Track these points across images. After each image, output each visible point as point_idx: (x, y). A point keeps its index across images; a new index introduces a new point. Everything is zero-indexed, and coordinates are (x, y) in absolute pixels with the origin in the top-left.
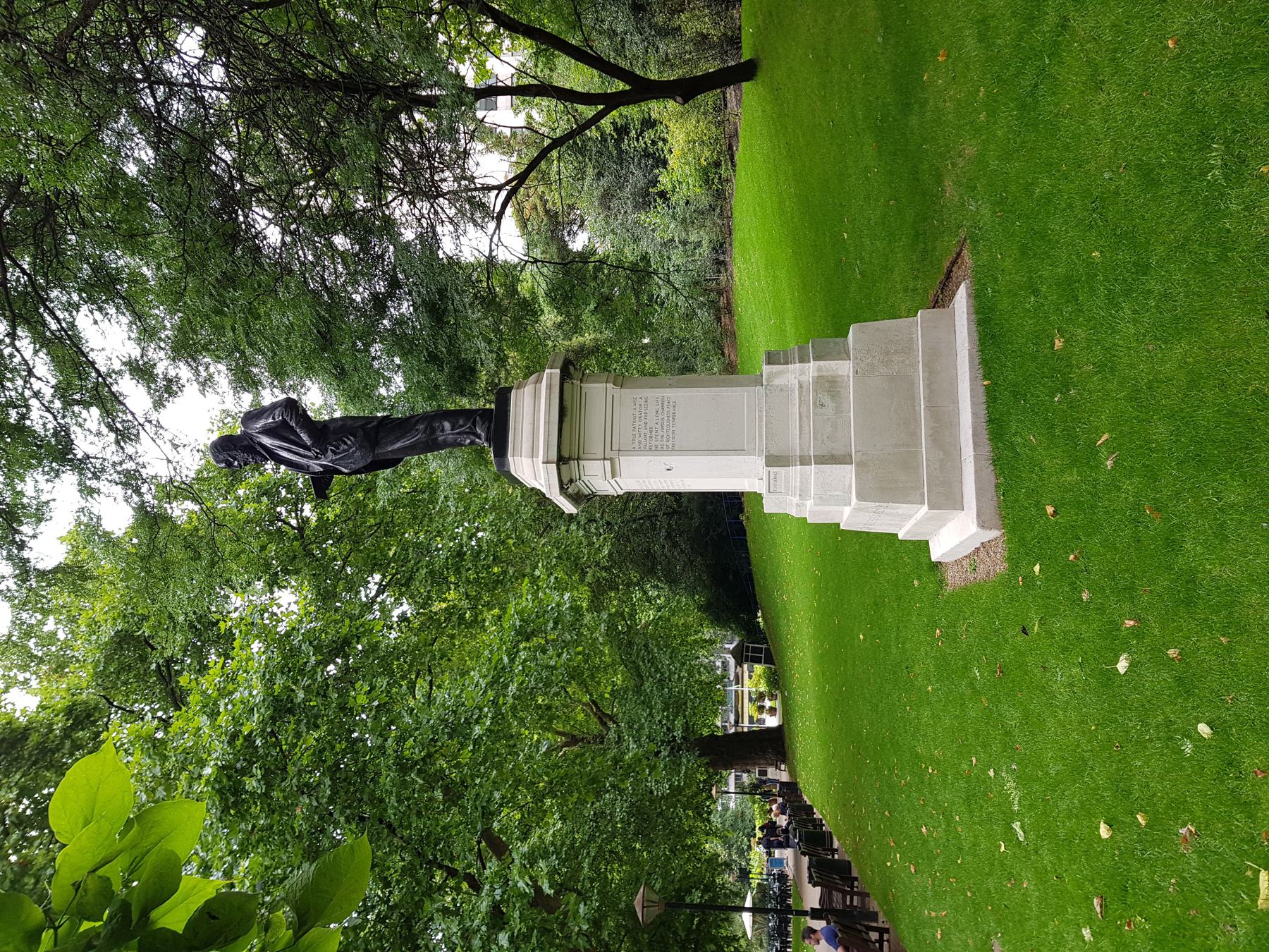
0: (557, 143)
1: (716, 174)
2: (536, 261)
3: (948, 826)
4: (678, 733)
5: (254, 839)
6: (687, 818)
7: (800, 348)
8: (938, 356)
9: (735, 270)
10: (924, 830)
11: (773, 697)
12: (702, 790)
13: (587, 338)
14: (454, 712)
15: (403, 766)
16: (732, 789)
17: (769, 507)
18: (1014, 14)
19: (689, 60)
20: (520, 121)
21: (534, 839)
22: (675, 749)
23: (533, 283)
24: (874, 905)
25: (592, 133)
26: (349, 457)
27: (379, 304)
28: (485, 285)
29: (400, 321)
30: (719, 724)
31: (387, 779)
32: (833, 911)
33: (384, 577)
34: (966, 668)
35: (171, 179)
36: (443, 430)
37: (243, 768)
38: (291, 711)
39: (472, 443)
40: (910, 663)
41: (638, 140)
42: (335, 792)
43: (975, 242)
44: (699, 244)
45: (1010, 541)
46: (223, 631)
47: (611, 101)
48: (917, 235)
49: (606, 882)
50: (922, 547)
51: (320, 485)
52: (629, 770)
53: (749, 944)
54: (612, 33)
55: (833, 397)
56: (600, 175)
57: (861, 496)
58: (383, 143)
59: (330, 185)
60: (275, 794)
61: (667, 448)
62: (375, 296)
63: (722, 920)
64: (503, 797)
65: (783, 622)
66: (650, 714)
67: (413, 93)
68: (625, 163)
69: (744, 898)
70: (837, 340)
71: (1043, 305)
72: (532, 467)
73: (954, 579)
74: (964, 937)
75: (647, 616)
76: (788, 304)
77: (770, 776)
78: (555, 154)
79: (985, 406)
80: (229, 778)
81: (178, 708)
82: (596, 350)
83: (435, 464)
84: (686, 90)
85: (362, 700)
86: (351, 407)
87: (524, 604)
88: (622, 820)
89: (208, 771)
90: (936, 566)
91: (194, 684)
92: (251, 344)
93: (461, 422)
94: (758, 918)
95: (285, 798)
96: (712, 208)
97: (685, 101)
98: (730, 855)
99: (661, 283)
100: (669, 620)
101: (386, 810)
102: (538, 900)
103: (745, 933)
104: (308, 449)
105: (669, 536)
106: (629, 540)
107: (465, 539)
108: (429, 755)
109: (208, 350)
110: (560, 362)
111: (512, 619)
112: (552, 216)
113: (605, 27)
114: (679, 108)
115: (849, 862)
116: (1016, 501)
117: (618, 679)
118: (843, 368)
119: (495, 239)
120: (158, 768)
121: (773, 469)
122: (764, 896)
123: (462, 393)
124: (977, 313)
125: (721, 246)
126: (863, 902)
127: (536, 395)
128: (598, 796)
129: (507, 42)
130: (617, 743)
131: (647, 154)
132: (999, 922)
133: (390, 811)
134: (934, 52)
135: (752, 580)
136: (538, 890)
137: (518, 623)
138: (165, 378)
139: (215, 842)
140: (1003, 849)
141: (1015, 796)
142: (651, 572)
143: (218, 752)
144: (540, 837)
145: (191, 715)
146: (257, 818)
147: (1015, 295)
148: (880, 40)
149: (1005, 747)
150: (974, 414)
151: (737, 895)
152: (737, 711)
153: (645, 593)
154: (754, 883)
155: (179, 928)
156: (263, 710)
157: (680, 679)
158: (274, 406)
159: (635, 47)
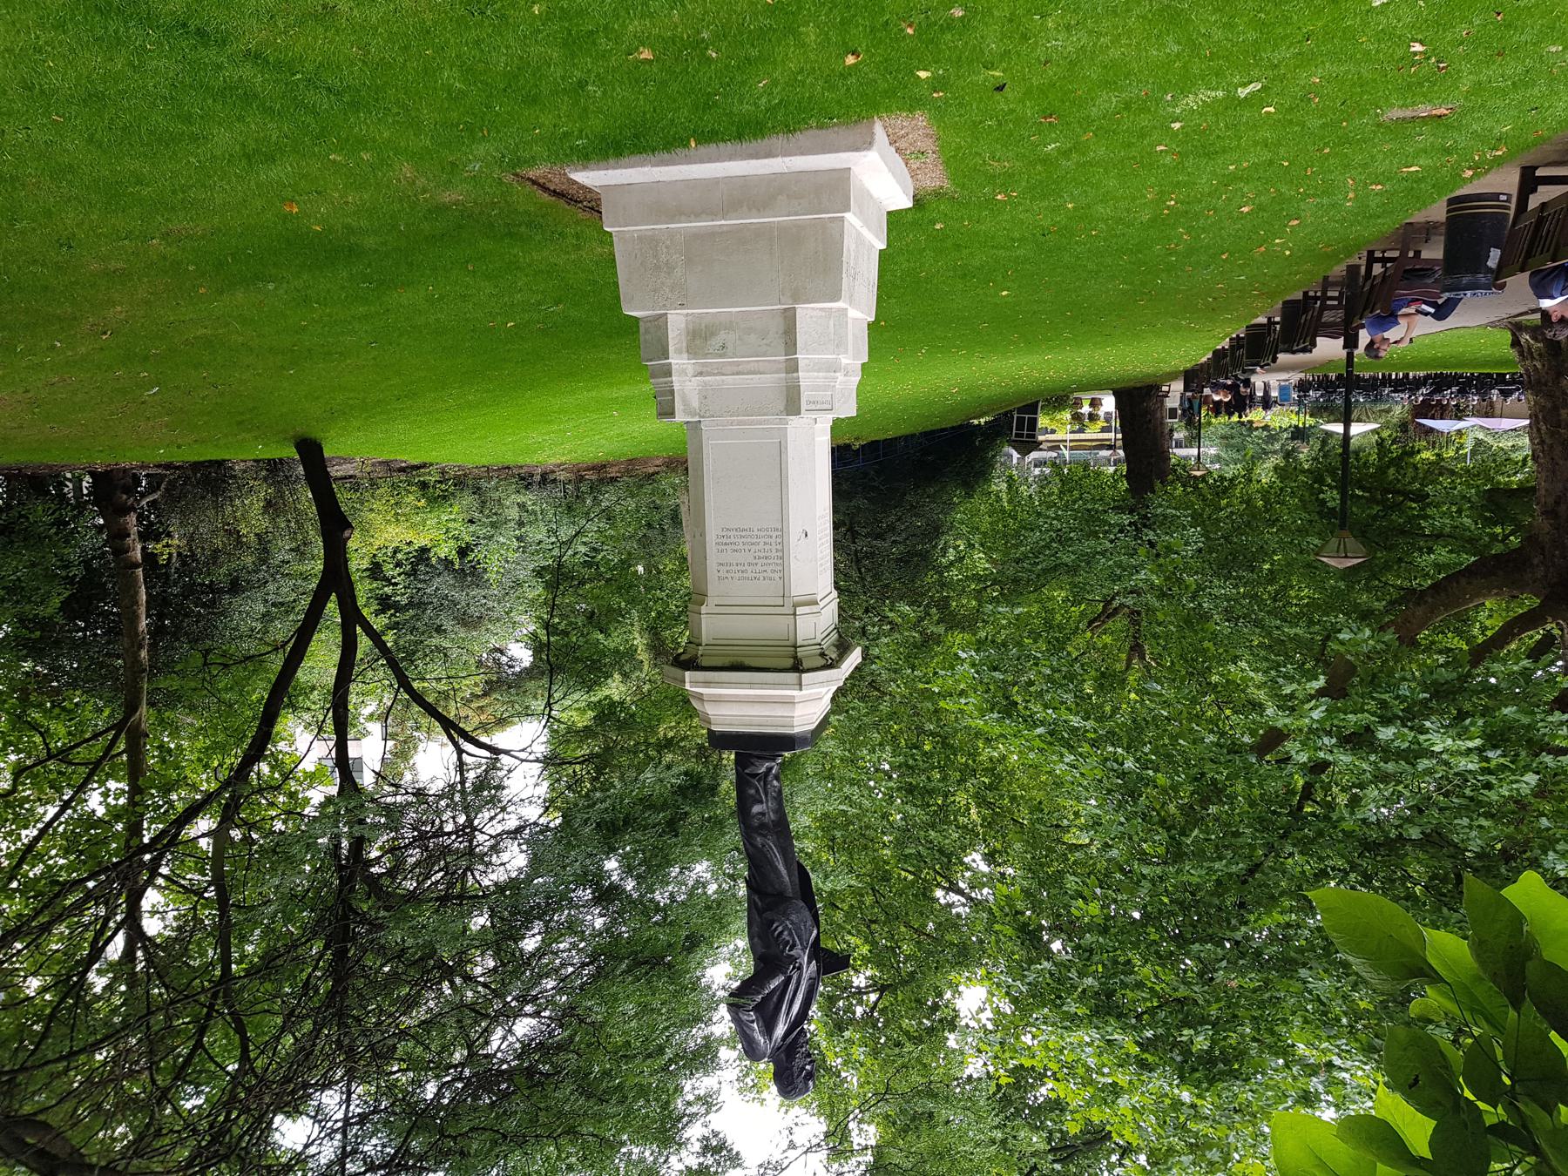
0: (404, 683)
1: (438, 487)
2: (549, 705)
3: (1241, 179)
4: (1126, 519)
5: (1269, 1040)
6: (1231, 506)
7: (653, 376)
8: (663, 204)
9: (553, 461)
10: (1245, 209)
11: (1078, 403)
12: (1196, 488)
13: (639, 641)
14: (1109, 792)
15: (1176, 854)
16: (1194, 451)
17: (849, 410)
18: (240, 119)
19: (297, 522)
20: (376, 728)
21: (1261, 695)
22: (1146, 522)
23: (575, 708)
24: (1339, 270)
25: (389, 638)
26: (798, 929)
27: (606, 895)
28: (578, 767)
29: (628, 870)
30: (1112, 469)
31: (1193, 873)
32: (1347, 321)
33: (938, 885)
34: (1046, 160)
35: (462, 1154)
36: (763, 814)
37: (1181, 1053)
38: (1110, 994)
39: (777, 777)
40: (1038, 232)
41: (396, 584)
42: (1210, 938)
43: (519, 162)
44: (522, 506)
45: (888, 109)
46: (1011, 1080)
47: (351, 617)
48: (510, 235)
49: (1313, 605)
50: (895, 220)
51: (833, 963)
52: (1173, 579)
53: (1386, 426)
54: (267, 618)
55: (713, 334)
56: (439, 630)
57: (836, 296)
58: (412, 897)
59: (463, 959)
60: (1214, 1011)
61: (778, 538)
62: (597, 901)
63: (1358, 460)
64: (1211, 731)
65: (985, 392)
66: (1103, 553)
67: (347, 858)
68: (425, 599)
69: (1329, 434)
70: (642, 330)
71: (598, 75)
72: (806, 704)
73: (935, 179)
74: (1381, 156)
75: (980, 562)
76: (594, 394)
77: (1176, 405)
78: (415, 685)
79: (722, 145)
80: (1194, 1070)
81: (1108, 1136)
82: (653, 631)
83: (800, 821)
84: (335, 526)
85: (1094, 908)
86: (733, 928)
87: (971, 707)
88: (1236, 586)
89: (1186, 1096)
90: (917, 201)
91: (1077, 1116)
92: (661, 1050)
93: (752, 792)
94: (1355, 415)
95: (1218, 1000)
96: (477, 490)
97: (349, 526)
98: (1275, 452)
99: (570, 552)
100: (984, 534)
101: (1230, 875)
102: (1335, 690)
103: (1374, 431)
104: (789, 979)
105: (880, 536)
106: (887, 586)
107: (891, 784)
108: (1162, 822)
109: (667, 1103)
110: (677, 672)
111: (989, 723)
112: (490, 687)
113: (259, 626)
114: (357, 533)
115: (1285, 303)
116: (839, 102)
117: (1060, 595)
118: (677, 322)
119: (523, 755)
120: (1183, 1158)
121: (804, 406)
122: (1326, 409)
123: (713, 789)
124: (606, 157)
125: (523, 479)
126: (1335, 284)
127: (717, 700)
128: (1206, 617)
129: (282, 746)
130: (1139, 595)
131: (413, 573)
132: (1363, 113)
133: (1234, 869)
134: (285, 218)
135: (933, 432)
136: (1321, 693)
137: (996, 715)
138: (704, 1154)
139: (1276, 1087)
140: (1272, 109)
141: (1206, 95)
142: (925, 556)
143: (1159, 1082)
144: (1259, 688)
145: (1117, 1119)
146: (1242, 1036)
147: (585, 109)
148: (271, 286)
149: (1144, 109)
150: (731, 158)
151: (1324, 443)
152: (1096, 448)
153: (952, 564)
154: (1310, 421)
155: (1430, 1124)
156: (1109, 1029)
157: (1057, 518)
158: (736, 1019)
159: (282, 590)
